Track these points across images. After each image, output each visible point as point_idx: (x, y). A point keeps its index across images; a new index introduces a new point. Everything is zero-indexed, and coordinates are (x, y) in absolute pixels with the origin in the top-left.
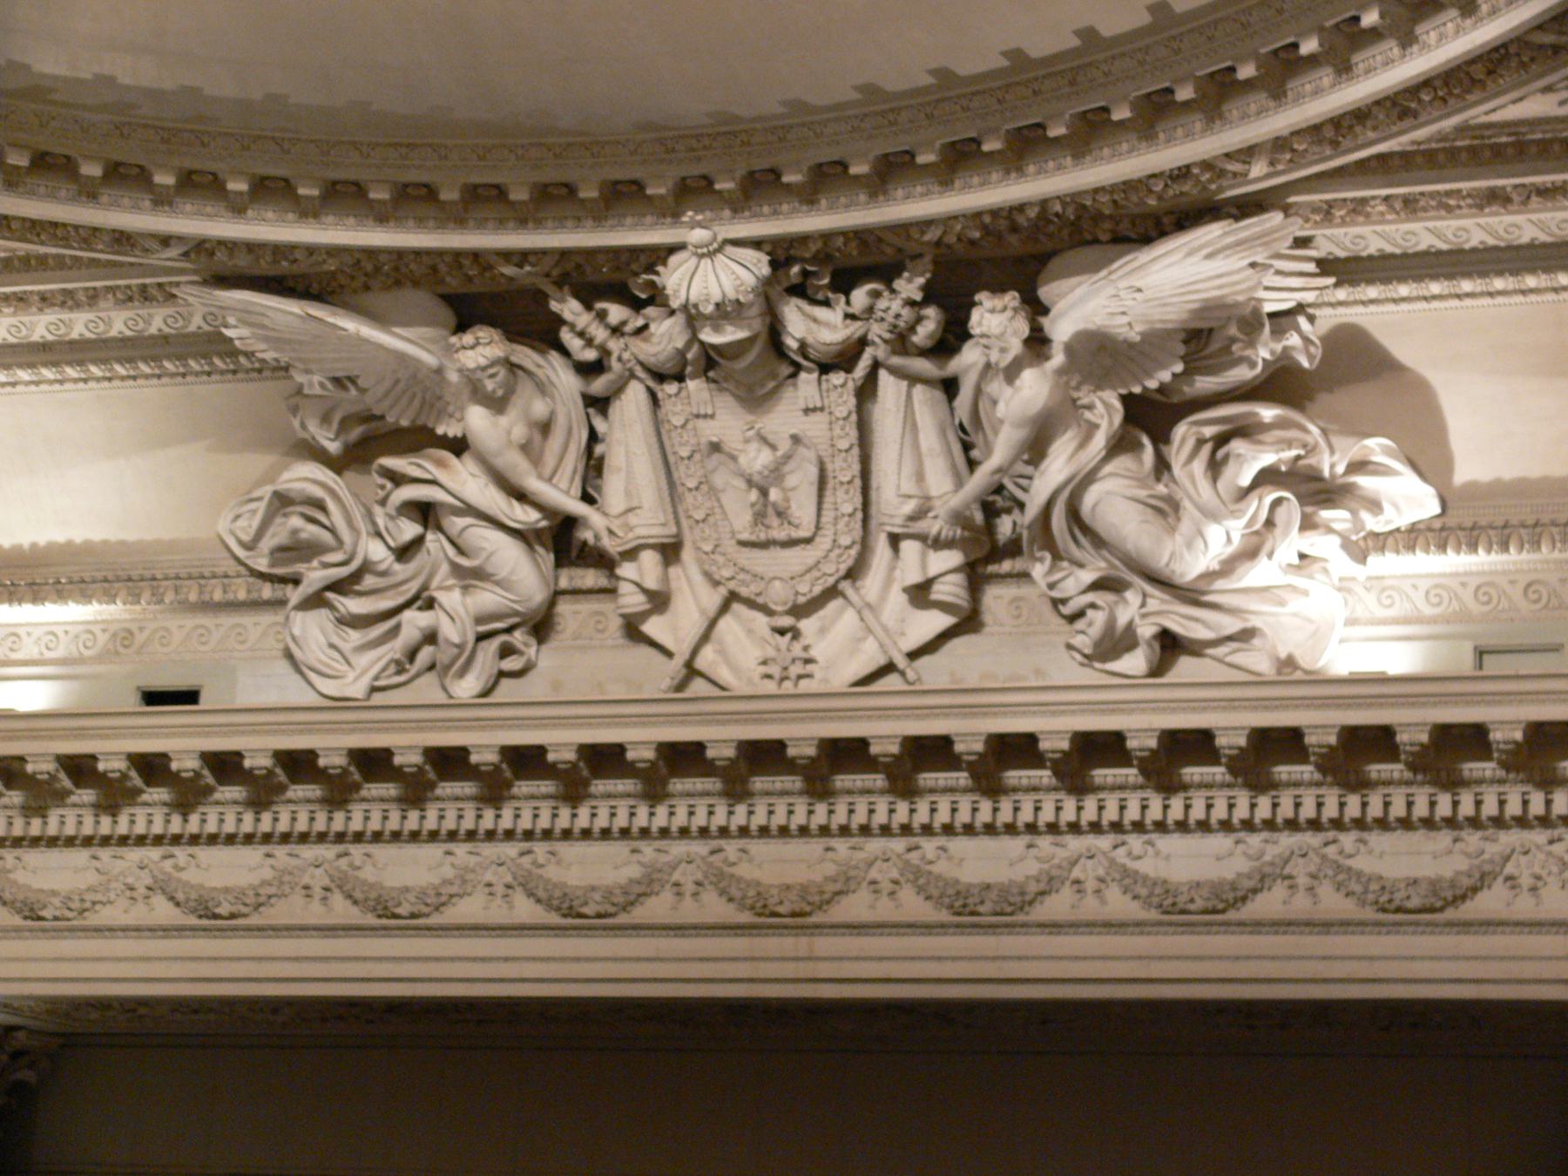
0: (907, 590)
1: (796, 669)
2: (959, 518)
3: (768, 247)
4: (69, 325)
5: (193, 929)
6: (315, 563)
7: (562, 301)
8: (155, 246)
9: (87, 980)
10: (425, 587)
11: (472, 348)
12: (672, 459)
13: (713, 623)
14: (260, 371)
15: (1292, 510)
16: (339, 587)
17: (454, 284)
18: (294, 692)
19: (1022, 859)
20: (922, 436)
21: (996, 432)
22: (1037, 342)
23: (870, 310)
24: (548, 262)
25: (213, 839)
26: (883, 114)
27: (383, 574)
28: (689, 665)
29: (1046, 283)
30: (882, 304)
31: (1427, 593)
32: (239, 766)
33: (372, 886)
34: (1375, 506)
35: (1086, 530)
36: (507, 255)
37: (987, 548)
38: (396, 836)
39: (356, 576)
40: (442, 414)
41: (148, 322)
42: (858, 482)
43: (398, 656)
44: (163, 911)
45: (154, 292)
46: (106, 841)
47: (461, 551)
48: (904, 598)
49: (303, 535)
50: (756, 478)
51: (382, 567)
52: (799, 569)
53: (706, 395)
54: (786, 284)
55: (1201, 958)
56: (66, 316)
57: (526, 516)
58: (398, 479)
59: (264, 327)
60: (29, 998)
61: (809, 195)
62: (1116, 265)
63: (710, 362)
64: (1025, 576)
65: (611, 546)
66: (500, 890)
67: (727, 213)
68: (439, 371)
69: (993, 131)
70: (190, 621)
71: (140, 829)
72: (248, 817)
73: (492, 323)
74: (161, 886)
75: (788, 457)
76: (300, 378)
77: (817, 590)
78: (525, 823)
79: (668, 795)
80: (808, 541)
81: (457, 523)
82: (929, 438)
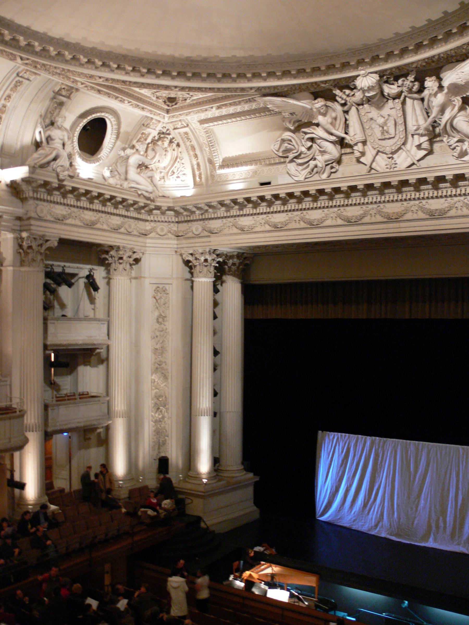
0: (416, 146)
1: (393, 166)
2: (426, 129)
3: (378, 73)
4: (236, 109)
5: (273, 231)
6: (291, 153)
7: (336, 91)
8: (249, 90)
9: (254, 242)
10: (314, 156)
11: (317, 103)
12: (363, 123)
13: (375, 158)
14: (276, 114)
16: (296, 157)
17: (312, 90)
18: (290, 180)
19: (444, 203)
20: (417, 112)
21: (433, 108)
22: (441, 87)
23: (403, 84)
24: (331, 82)
25: (276, 212)
26: (400, 39)
27: (305, 154)
28: (370, 167)
29: (442, 73)
30: (405, 83)
32: (279, 196)
33: (308, 219)
35: (455, 129)
36: (322, 82)
37: (434, 135)
38: (312, 208)
39: (300, 155)
40: (314, 118)
41: (252, 106)
42: (403, 123)
43: (310, 171)
44: (268, 228)
45: (251, 100)
46: (255, 214)
47: (320, 147)
48: (416, 148)
49: (288, 147)
50: (381, 125)
51: (305, 152)
52: (392, 144)
53: (369, 108)
54: (384, 81)
56: (236, 107)
57: (333, 138)
58: (306, 133)
59: (274, 104)
60: (244, 247)
61: (386, 60)
62: (456, 67)
63: (369, 100)
64: (442, 141)
65: (352, 143)
66: (334, 218)
67: (369, 66)
68: (311, 109)
69: (425, 39)
70: (268, 168)
71: (261, 211)
72: (282, 207)
73: (321, 97)
74: (267, 223)
75: (387, 119)
76: (284, 114)
77: (396, 148)
78: (338, 204)
79: (385, 194)
80: (393, 138)
81: (318, 141)
82: (418, 112)
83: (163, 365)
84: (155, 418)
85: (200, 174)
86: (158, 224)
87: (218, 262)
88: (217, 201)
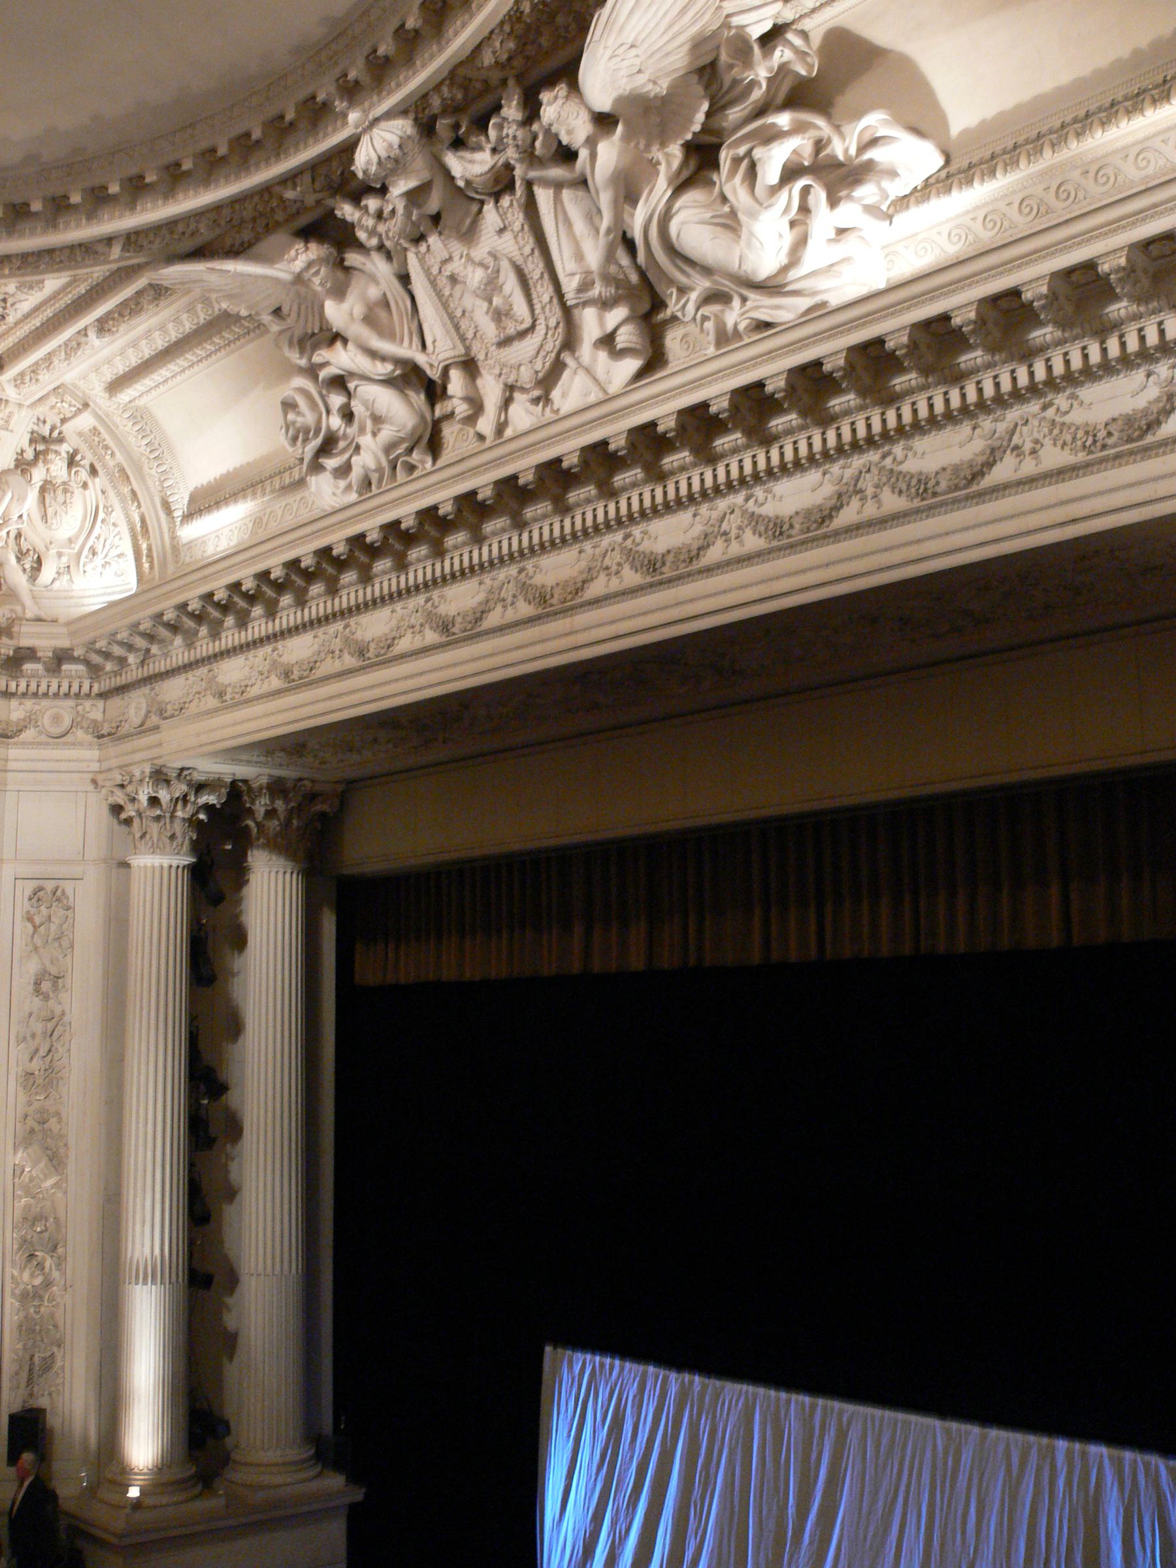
15: (819, 195)
31: (949, 234)
34: (893, 174)
55: (803, 571)
57: (384, 369)
83: (53, 1123)
84: (22, 1287)
85: (150, 549)
86: (45, 703)
87: (208, 808)
88: (151, 617)
